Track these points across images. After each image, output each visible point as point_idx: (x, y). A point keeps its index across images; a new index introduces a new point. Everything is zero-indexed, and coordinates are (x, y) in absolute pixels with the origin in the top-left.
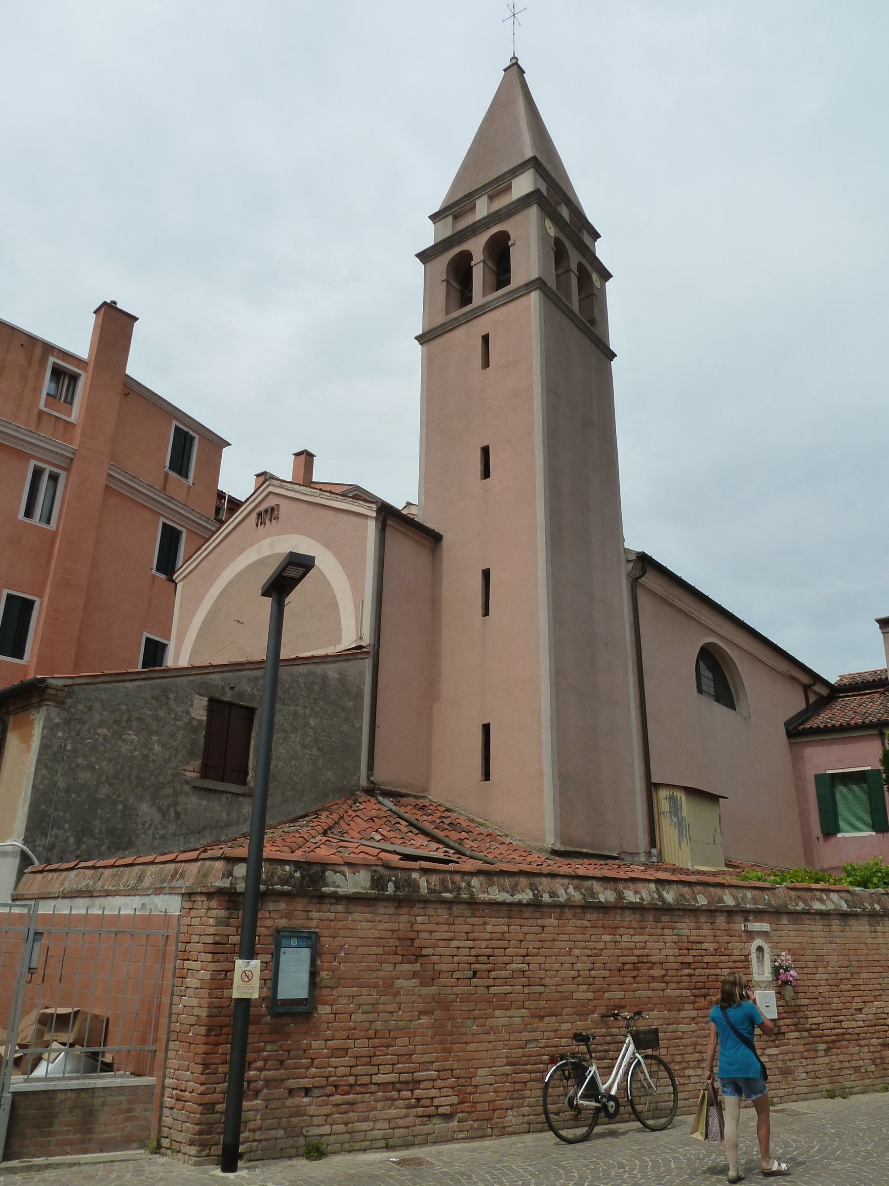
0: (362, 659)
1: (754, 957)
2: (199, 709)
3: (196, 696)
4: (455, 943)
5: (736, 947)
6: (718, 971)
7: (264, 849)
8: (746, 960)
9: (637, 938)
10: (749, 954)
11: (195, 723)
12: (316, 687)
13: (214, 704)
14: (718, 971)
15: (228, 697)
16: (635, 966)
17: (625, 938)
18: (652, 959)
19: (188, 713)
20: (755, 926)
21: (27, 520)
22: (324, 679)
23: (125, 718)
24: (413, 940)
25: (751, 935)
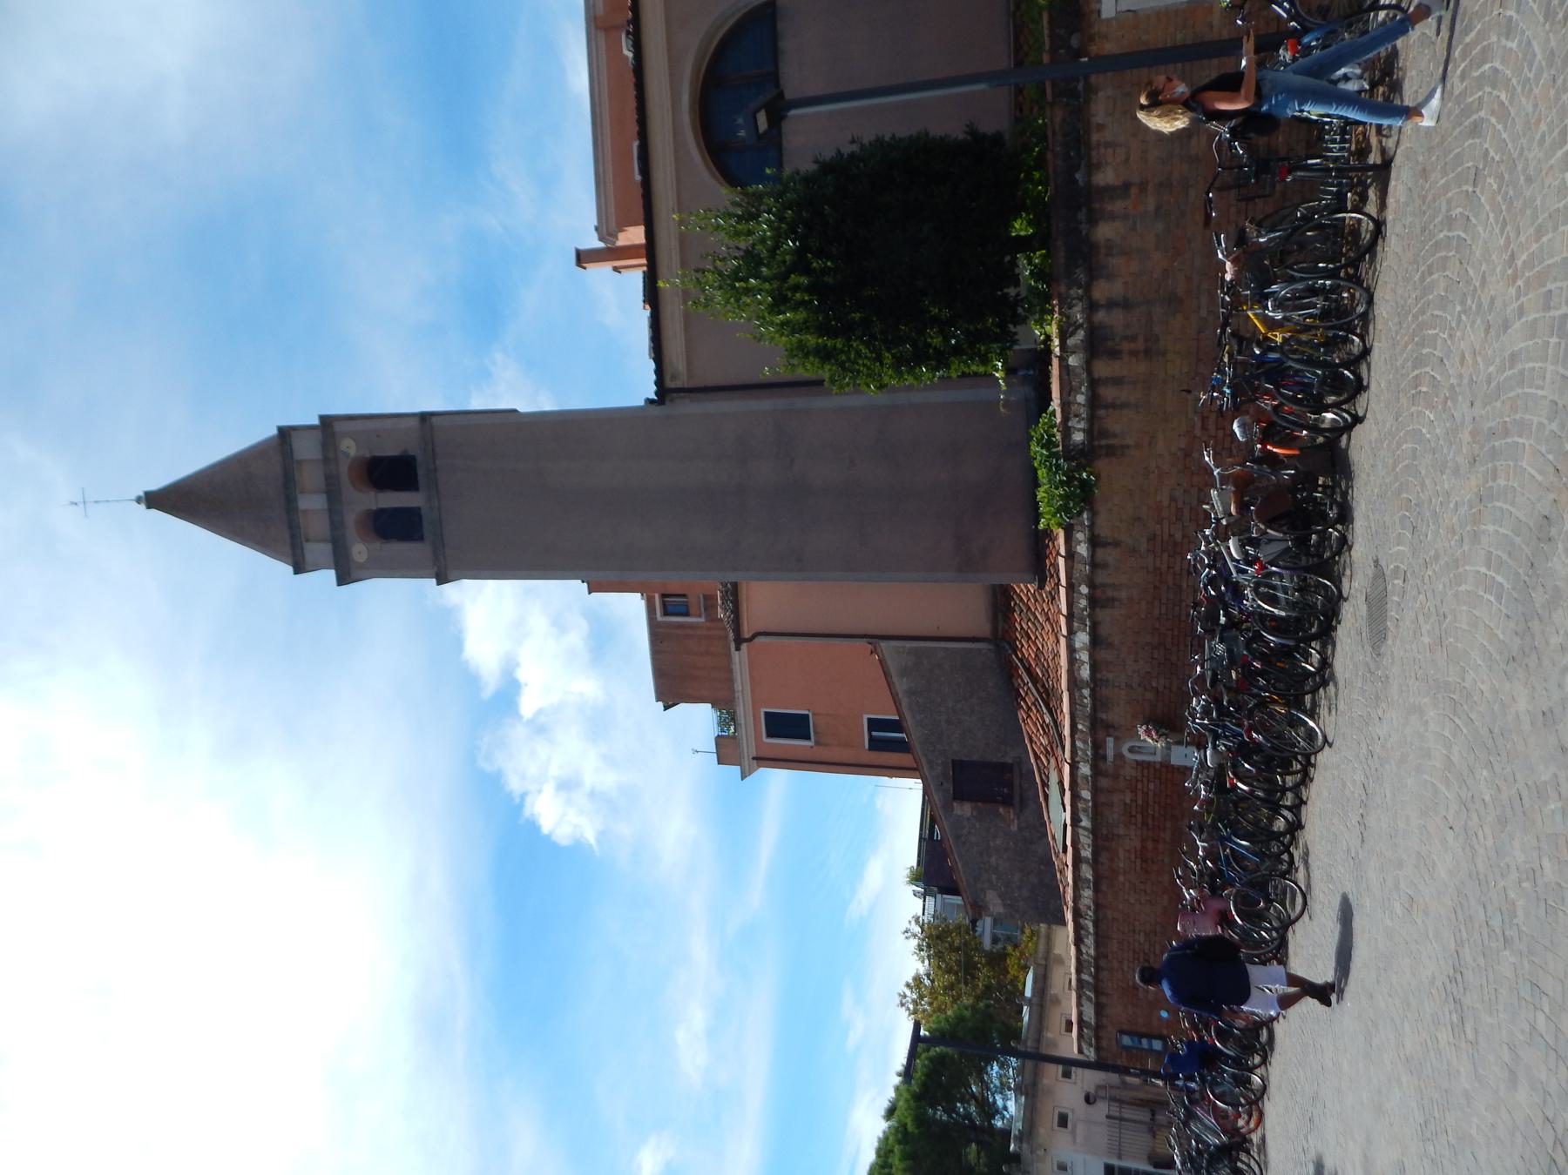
0: (882, 651)
1: (1139, 758)
2: (965, 810)
3: (955, 812)
4: (1126, 969)
5: (1129, 772)
6: (1151, 794)
7: (1052, 403)
8: (1140, 764)
9: (1122, 856)
10: (1136, 761)
11: (975, 813)
12: (921, 701)
13: (960, 796)
14: (1151, 794)
15: (949, 786)
16: (1144, 860)
17: (1121, 865)
18: (1139, 846)
19: (968, 819)
20: (1110, 753)
21: (731, 577)
22: (911, 693)
23: (982, 866)
24: (1191, 509)
25: (1119, 756)
